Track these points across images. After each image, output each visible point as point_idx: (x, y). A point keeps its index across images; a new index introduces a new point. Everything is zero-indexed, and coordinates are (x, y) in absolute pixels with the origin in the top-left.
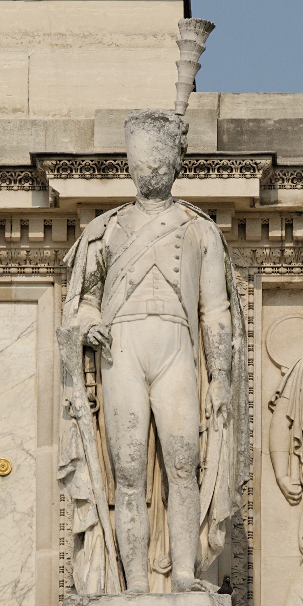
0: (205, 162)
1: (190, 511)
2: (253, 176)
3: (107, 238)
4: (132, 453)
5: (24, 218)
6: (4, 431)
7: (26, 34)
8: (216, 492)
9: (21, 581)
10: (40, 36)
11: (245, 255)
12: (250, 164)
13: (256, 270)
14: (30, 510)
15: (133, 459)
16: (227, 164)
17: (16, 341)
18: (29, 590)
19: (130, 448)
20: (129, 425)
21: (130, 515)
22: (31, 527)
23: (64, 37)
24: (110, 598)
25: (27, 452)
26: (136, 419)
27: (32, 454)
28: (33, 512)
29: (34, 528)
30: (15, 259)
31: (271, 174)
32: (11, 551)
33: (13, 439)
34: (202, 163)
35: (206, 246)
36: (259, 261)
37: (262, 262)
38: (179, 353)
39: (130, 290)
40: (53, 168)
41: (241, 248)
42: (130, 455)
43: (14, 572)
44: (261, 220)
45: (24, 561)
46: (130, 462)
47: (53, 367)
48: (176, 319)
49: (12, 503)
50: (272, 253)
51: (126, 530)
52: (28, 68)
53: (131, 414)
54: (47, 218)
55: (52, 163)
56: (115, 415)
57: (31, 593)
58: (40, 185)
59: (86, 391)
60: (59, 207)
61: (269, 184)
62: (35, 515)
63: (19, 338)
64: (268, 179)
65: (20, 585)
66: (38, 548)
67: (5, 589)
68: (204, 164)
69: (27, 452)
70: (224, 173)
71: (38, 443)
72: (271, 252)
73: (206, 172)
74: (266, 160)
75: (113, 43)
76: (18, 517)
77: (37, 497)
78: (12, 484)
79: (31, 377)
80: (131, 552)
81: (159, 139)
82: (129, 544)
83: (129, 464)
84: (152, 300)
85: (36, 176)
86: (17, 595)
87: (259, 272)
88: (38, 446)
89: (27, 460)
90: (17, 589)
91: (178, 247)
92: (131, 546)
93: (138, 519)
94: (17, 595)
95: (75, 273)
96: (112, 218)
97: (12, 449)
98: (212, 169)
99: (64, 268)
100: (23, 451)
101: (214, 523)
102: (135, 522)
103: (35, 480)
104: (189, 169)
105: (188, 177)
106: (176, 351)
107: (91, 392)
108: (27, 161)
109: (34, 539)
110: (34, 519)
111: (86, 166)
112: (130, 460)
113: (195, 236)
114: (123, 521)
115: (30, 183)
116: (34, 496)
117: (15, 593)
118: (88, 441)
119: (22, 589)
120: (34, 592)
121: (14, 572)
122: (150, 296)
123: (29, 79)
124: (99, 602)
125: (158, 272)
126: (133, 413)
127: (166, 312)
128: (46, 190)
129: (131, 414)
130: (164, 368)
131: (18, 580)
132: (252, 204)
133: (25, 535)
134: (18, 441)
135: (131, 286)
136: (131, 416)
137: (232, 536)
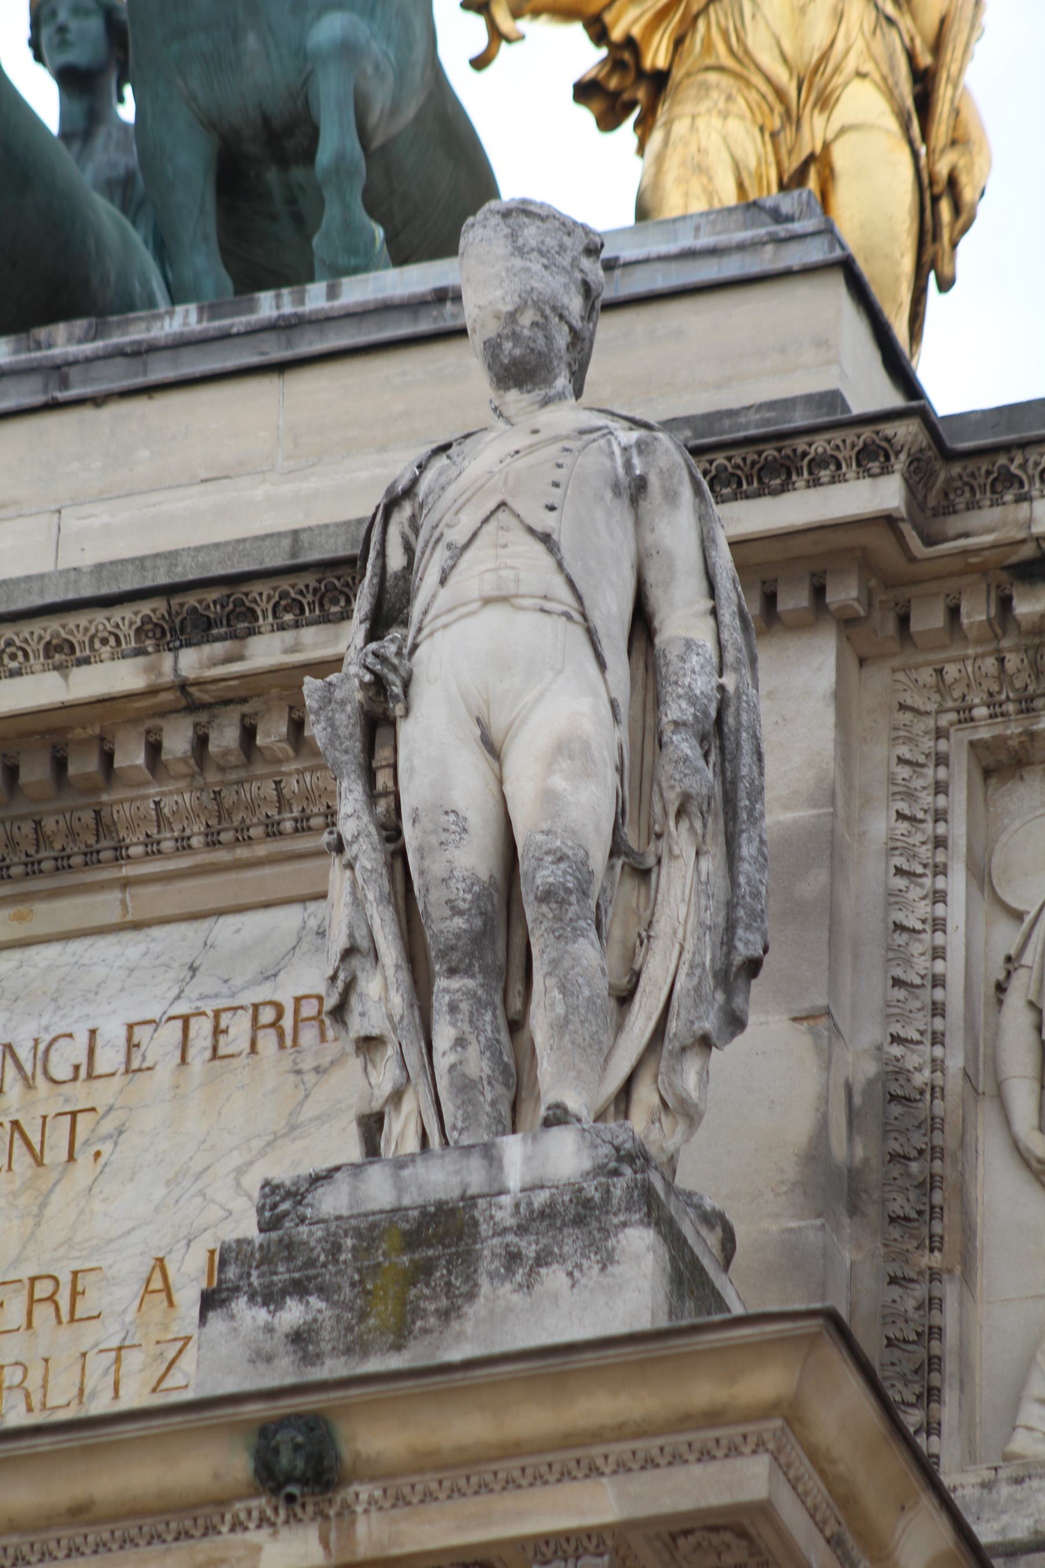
0: (776, 454)
2: (886, 470)
8: (678, 986)
11: (921, 683)
13: (953, 716)
15: (456, 912)
16: (825, 451)
34: (770, 458)
36: (957, 694)
37: (964, 696)
41: (910, 670)
44: (942, 596)
46: (451, 918)
48: (548, 605)
53: (446, 813)
61: (944, 503)
68: (775, 458)
70: (823, 473)
72: (976, 666)
73: (784, 477)
74: (908, 426)
84: (492, 570)
87: (960, 722)
93: (474, 1042)
98: (797, 469)
101: (327, 700)
104: (747, 477)
105: (747, 497)
112: (448, 913)
118: (375, 905)
122: (490, 565)
126: (453, 811)
127: (523, 590)
136: (446, 818)
137: (885, 1239)
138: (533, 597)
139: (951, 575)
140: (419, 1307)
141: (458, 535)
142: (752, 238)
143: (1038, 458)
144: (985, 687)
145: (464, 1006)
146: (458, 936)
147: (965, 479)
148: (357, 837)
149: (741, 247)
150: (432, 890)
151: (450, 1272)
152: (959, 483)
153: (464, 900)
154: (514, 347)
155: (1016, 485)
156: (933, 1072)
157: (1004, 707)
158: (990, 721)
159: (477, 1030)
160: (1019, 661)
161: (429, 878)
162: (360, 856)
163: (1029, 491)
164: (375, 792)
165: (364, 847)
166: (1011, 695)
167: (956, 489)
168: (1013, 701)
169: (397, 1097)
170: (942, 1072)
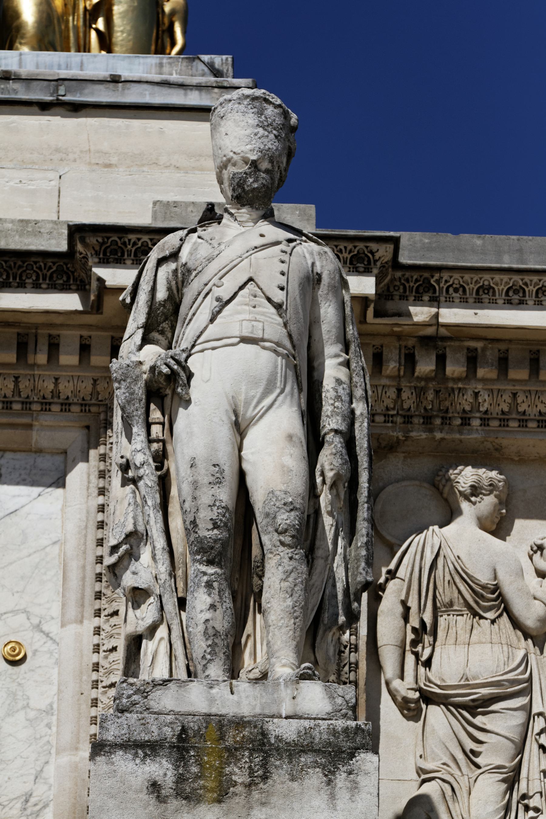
1: (296, 589)
3: (184, 256)
4: (214, 518)
5: (54, 332)
6: (17, 608)
7: (58, 150)
9: (34, 794)
10: (75, 153)
12: (364, 253)
14: (49, 707)
17: (35, 499)
18: (45, 806)
19: (212, 510)
20: (212, 479)
21: (209, 600)
22: (50, 728)
23: (107, 155)
24: (183, 684)
25: (47, 635)
26: (222, 472)
27: (54, 638)
28: (52, 709)
29: (54, 729)
30: (39, 388)
31: (389, 277)
32: (21, 757)
33: (28, 619)
35: (319, 272)
38: (281, 398)
39: (217, 309)
40: (97, 248)
42: (211, 519)
43: (25, 782)
44: (371, 346)
45: (39, 769)
46: (213, 529)
47: (86, 527)
48: (280, 349)
49: (24, 697)
50: (386, 393)
51: (203, 620)
52: (58, 189)
54: (85, 333)
55: (97, 241)
56: (191, 467)
57: (47, 810)
58: (78, 283)
59: (149, 448)
60: (102, 313)
62: (56, 713)
63: (39, 495)
64: (385, 285)
65: (33, 800)
66: (58, 753)
67: (11, 805)
69: (47, 635)
71: (62, 622)
75: (171, 164)
76: (32, 714)
77: (59, 689)
78: (25, 673)
79: (55, 543)
80: (209, 650)
81: (260, 124)
82: (207, 639)
83: (210, 532)
85: (73, 270)
86: (29, 812)
88: (63, 625)
89: (46, 645)
90: (29, 804)
91: (283, 262)
92: (210, 642)
93: (220, 607)
94: (29, 812)
95: (138, 303)
96: (190, 235)
97: (26, 630)
99: (104, 405)
100: (42, 634)
102: (215, 611)
103: (56, 670)
106: (278, 391)
107: (157, 448)
108: (63, 246)
109: (54, 743)
110: (55, 718)
111: (143, 248)
112: (211, 526)
113: (305, 257)
114: (198, 610)
115: (65, 278)
116: (55, 689)
117: (25, 809)
118: (152, 509)
119: (36, 805)
120: (51, 809)
121: (25, 782)
123: (59, 203)
124: (167, 689)
125: (257, 289)
127: (266, 337)
128: (85, 290)
129: (214, 465)
130: (261, 409)
131: (29, 793)
132: (362, 320)
133: (41, 737)
134: (35, 621)
135: (217, 303)
138: (271, 342)
139: (384, 335)
140: (231, 779)
141: (225, 293)
142: (206, 82)
143: (448, 279)
144: (385, 404)
145: (215, 584)
146: (215, 541)
147: (403, 281)
148: (143, 465)
149: (199, 87)
150: (201, 510)
151: (251, 762)
152: (398, 283)
153: (221, 520)
154: (254, 181)
155: (431, 291)
156: (351, 635)
157: (395, 419)
158: (383, 424)
159: (222, 602)
160: (410, 393)
161: (199, 502)
162: (145, 477)
163: (439, 296)
164: (150, 438)
165: (147, 472)
166: (400, 412)
167: (395, 286)
168: (401, 415)
169: (152, 630)
170: (356, 636)
